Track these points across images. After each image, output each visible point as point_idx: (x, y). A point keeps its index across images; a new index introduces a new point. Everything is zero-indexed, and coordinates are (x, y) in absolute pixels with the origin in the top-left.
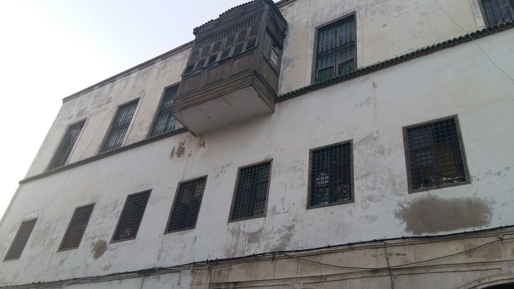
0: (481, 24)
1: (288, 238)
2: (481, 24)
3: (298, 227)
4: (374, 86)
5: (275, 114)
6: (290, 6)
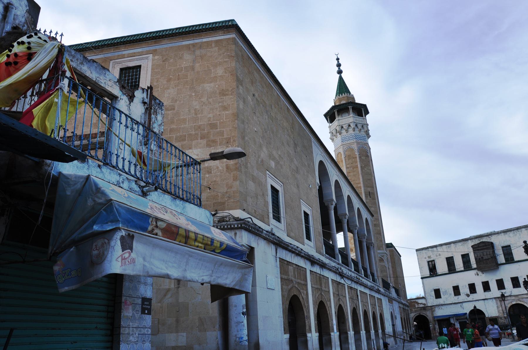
0: (447, 272)
1: (511, 293)
2: (447, 272)
3: (512, 291)
4: (519, 266)
5: (499, 268)
6: (491, 236)
